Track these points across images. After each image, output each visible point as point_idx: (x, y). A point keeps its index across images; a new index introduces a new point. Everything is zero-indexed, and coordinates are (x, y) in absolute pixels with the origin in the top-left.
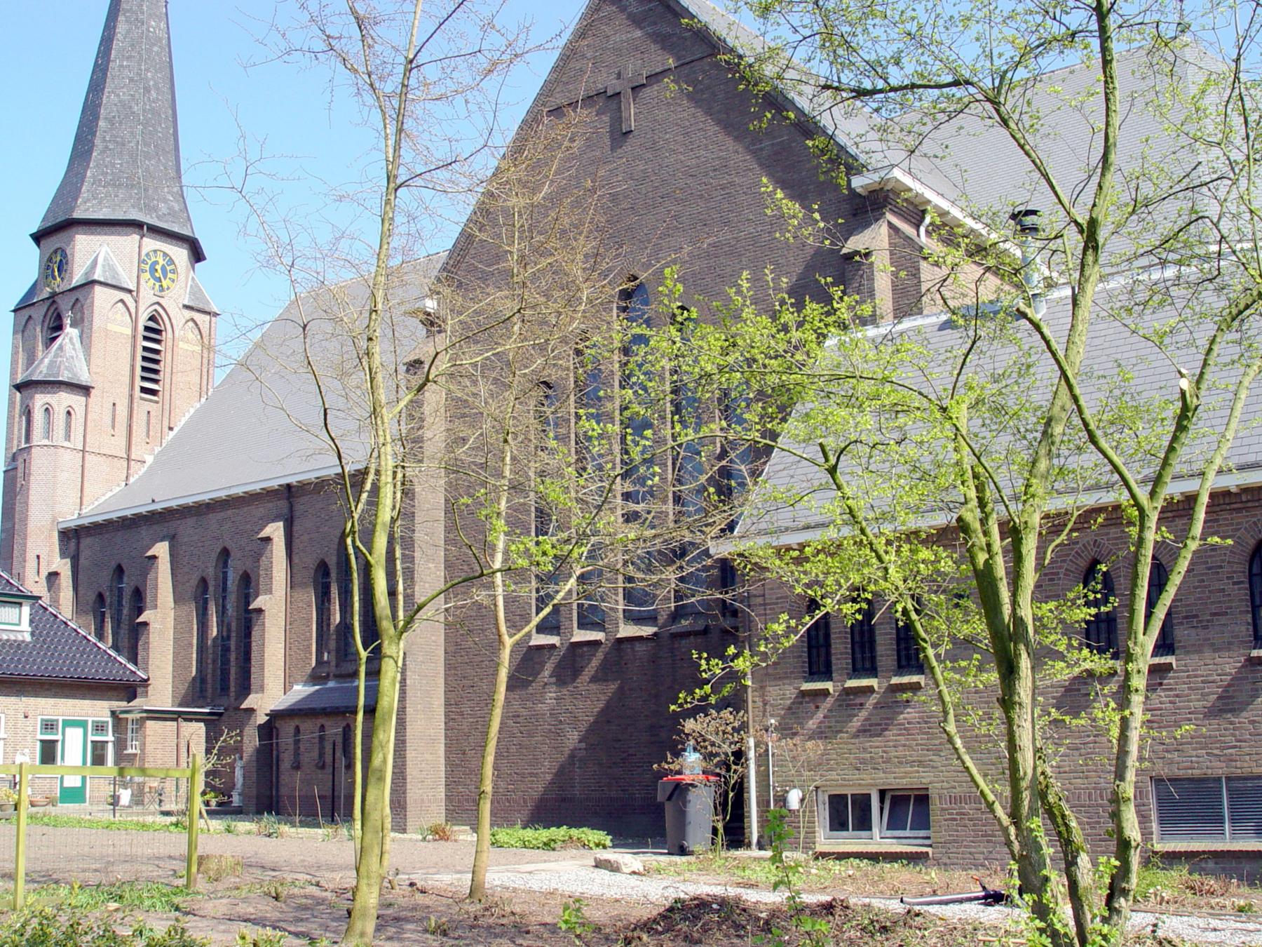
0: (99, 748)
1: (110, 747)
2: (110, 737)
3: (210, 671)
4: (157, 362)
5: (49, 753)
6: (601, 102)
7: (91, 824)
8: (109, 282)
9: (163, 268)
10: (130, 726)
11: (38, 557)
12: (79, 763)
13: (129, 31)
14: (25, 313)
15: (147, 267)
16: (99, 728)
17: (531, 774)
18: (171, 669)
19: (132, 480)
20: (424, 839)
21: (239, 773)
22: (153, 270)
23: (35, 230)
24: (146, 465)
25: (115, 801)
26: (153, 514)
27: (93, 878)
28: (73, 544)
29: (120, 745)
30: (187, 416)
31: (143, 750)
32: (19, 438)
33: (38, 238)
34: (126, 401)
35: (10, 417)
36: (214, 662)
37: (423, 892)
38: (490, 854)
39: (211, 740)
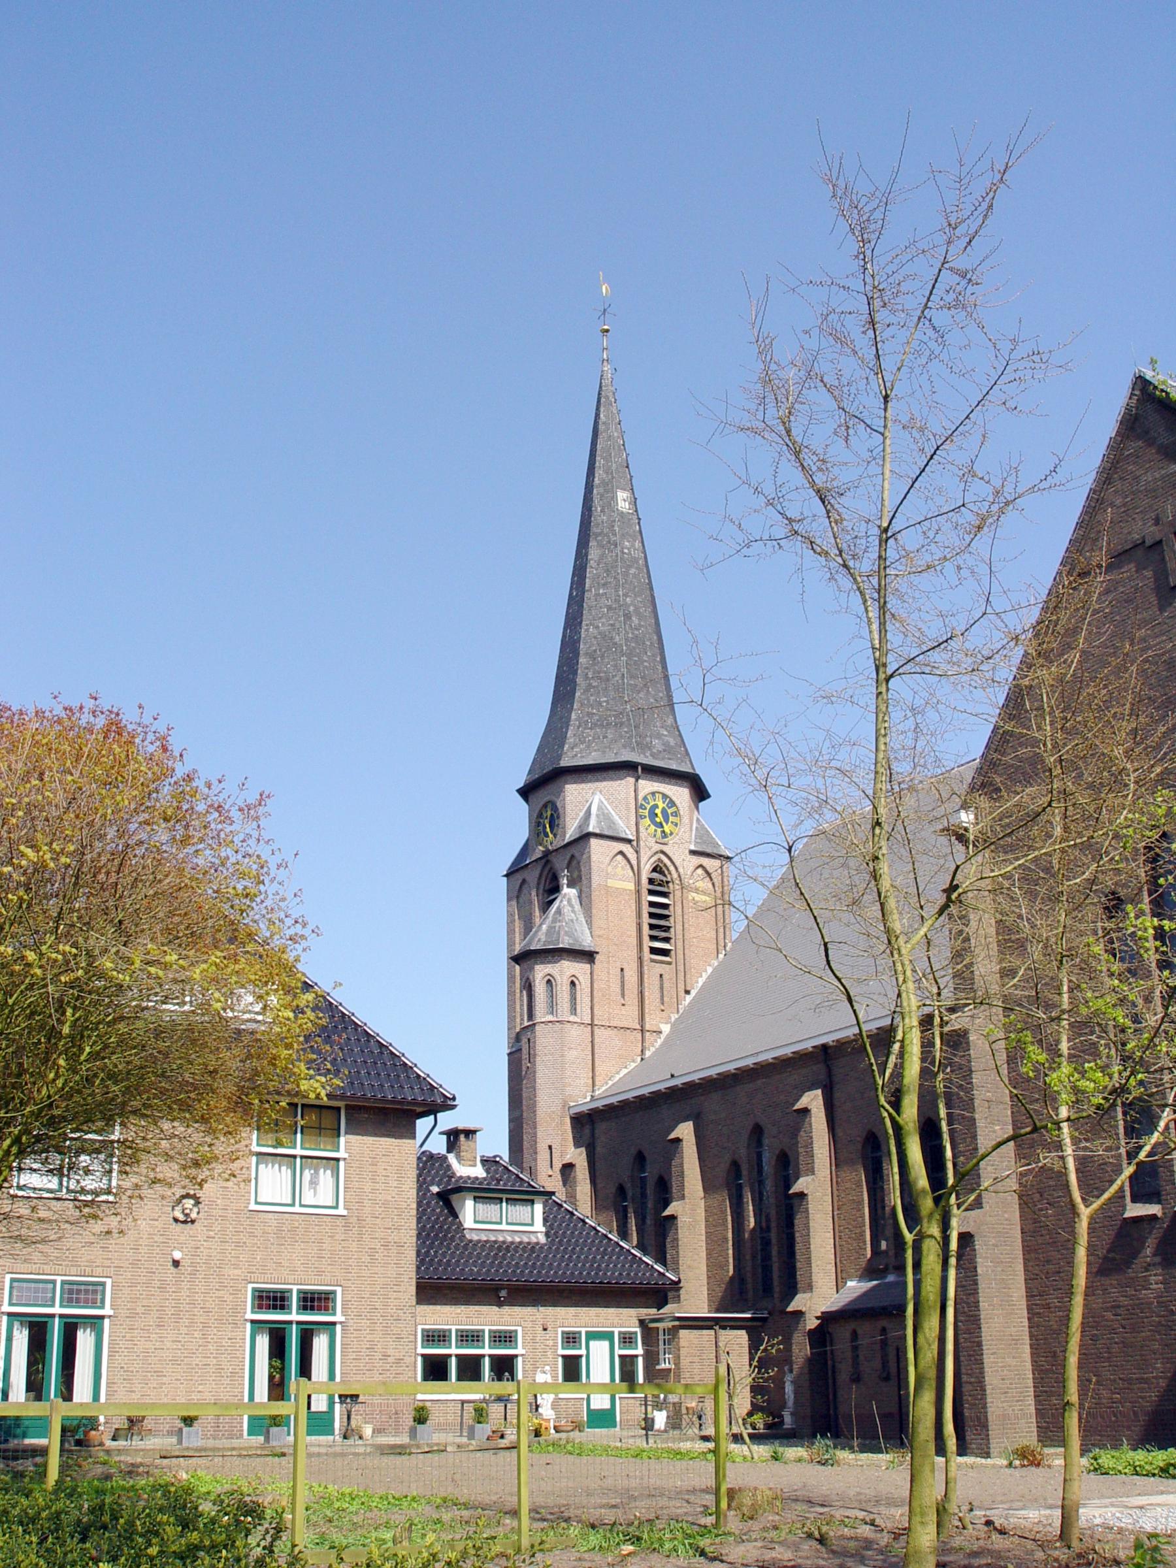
0: (627, 1363)
2: (639, 1351)
3: (749, 1269)
4: (666, 917)
5: (572, 1369)
6: (1139, 553)
7: (618, 1453)
8: (606, 833)
9: (664, 811)
10: (661, 1337)
11: (550, 1147)
12: (607, 1380)
13: (602, 556)
14: (519, 877)
15: (646, 813)
16: (627, 1340)
17: (1141, 1380)
18: (705, 1268)
19: (648, 1054)
20: (1010, 1465)
21: (789, 1388)
23: (522, 785)
24: (663, 1036)
25: (648, 1424)
26: (673, 1090)
27: (609, 1516)
28: (587, 1131)
29: (651, 1358)
30: (705, 976)
31: (677, 1364)
32: (522, 1015)
33: (526, 792)
35: (511, 993)
36: (754, 1257)
37: (1002, 1532)
38: (1085, 1484)
39: (754, 1346)
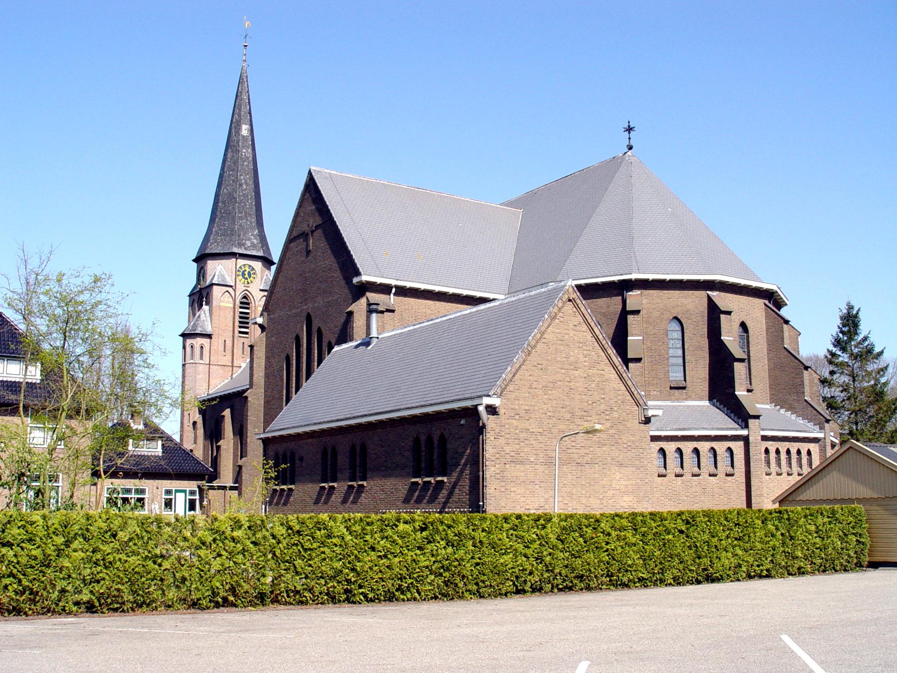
1: (198, 502)
2: (197, 497)
4: (248, 318)
5: (168, 504)
13: (233, 156)
14: (192, 298)
16: (192, 493)
22: (243, 274)
34: (231, 339)
